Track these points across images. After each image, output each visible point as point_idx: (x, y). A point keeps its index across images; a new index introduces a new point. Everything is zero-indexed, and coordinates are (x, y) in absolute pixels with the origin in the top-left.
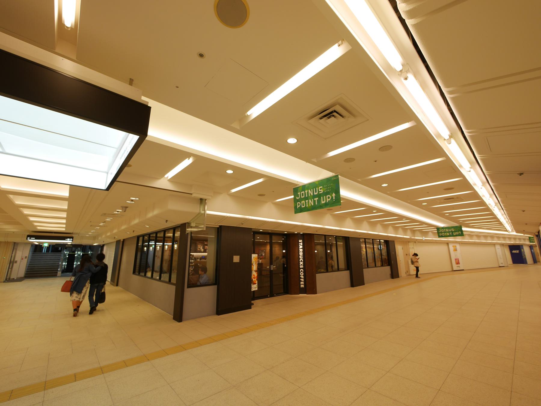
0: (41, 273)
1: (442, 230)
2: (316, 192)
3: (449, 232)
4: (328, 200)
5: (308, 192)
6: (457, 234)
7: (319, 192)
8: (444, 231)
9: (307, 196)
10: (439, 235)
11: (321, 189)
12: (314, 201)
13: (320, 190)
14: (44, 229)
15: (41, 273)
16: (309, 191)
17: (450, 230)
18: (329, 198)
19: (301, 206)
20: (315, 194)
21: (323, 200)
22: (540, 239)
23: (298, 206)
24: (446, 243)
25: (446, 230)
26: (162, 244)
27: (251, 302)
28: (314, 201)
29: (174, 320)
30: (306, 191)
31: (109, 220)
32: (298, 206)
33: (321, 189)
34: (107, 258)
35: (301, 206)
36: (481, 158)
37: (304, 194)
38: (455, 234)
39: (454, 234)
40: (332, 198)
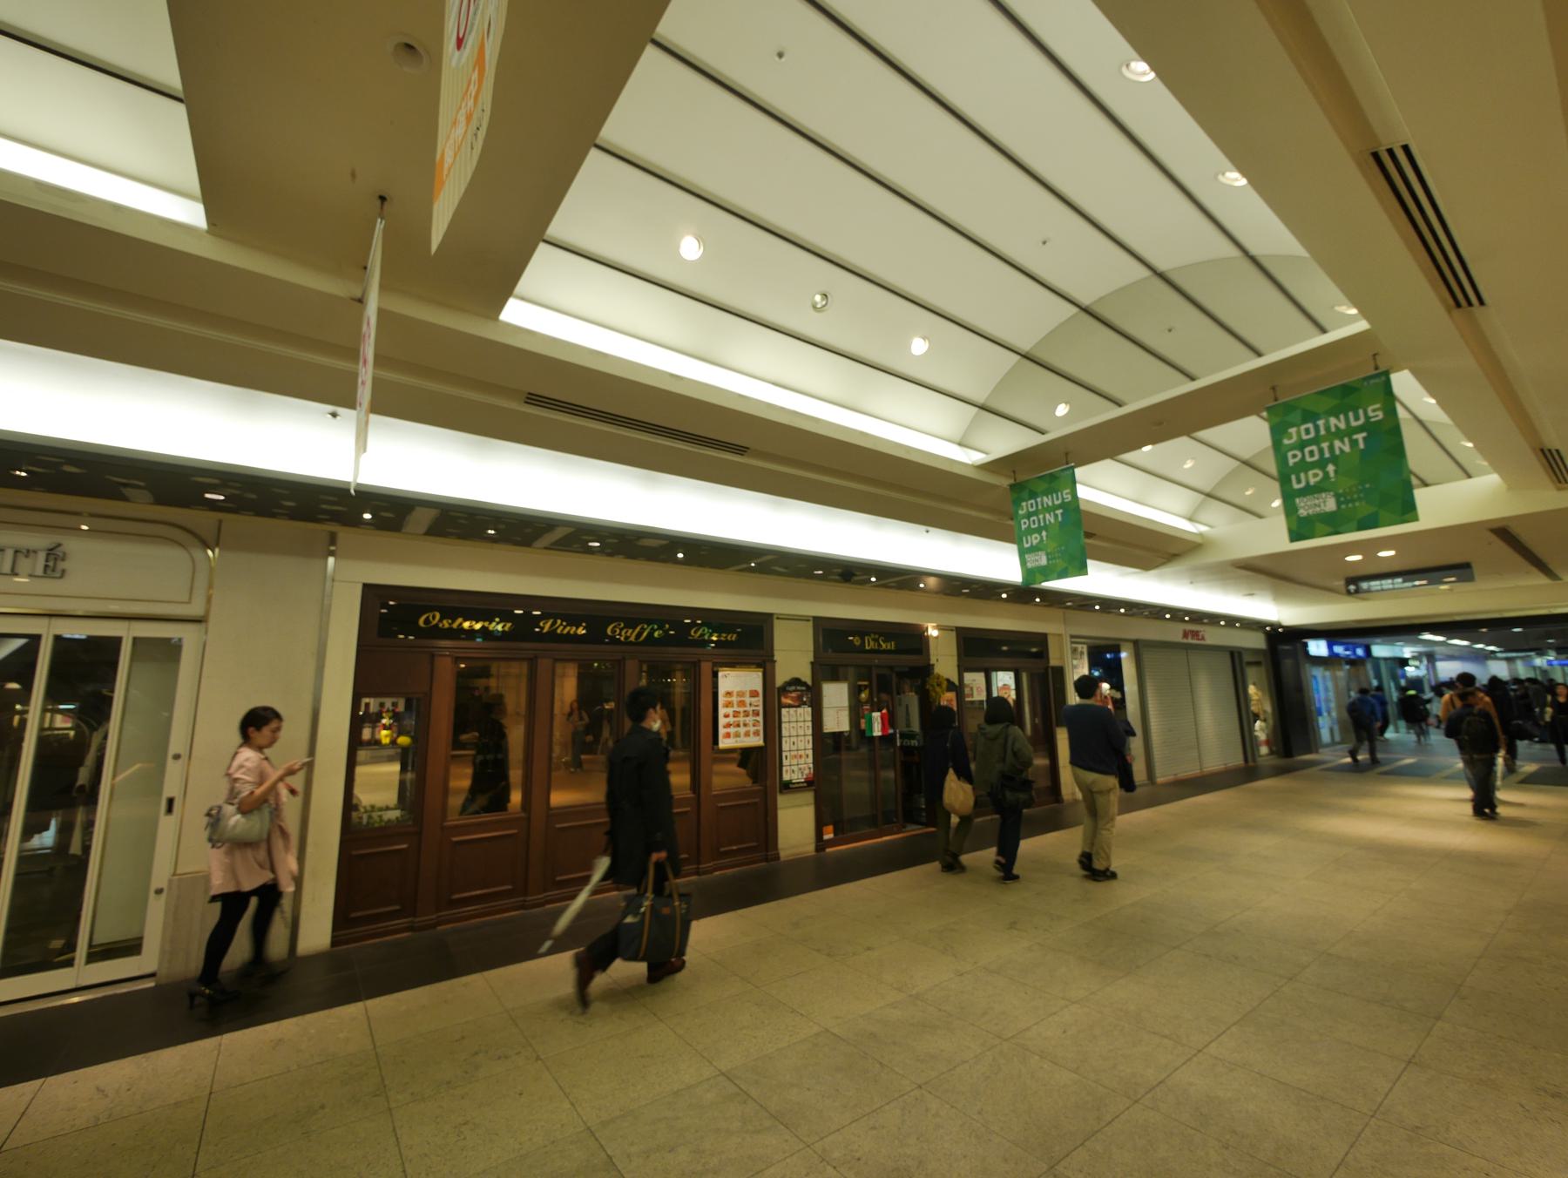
1: (1303, 427)
2: (1058, 499)
3: (1350, 431)
5: (1331, 448)
6: (1312, 481)
7: (1063, 499)
8: (1321, 451)
9: (1042, 524)
10: (1296, 509)
11: (1067, 494)
12: (1056, 516)
13: (1065, 496)
14: (692, 447)
16: (1047, 516)
17: (1357, 419)
18: (1036, 538)
21: (1027, 543)
22: (1565, 466)
24: (382, 208)
25: (1333, 421)
28: (1056, 516)
29: (945, 874)
30: (1041, 516)
31: (62, 707)
33: (1067, 494)
37: (895, 693)
38: (1302, 485)
39: (1296, 486)
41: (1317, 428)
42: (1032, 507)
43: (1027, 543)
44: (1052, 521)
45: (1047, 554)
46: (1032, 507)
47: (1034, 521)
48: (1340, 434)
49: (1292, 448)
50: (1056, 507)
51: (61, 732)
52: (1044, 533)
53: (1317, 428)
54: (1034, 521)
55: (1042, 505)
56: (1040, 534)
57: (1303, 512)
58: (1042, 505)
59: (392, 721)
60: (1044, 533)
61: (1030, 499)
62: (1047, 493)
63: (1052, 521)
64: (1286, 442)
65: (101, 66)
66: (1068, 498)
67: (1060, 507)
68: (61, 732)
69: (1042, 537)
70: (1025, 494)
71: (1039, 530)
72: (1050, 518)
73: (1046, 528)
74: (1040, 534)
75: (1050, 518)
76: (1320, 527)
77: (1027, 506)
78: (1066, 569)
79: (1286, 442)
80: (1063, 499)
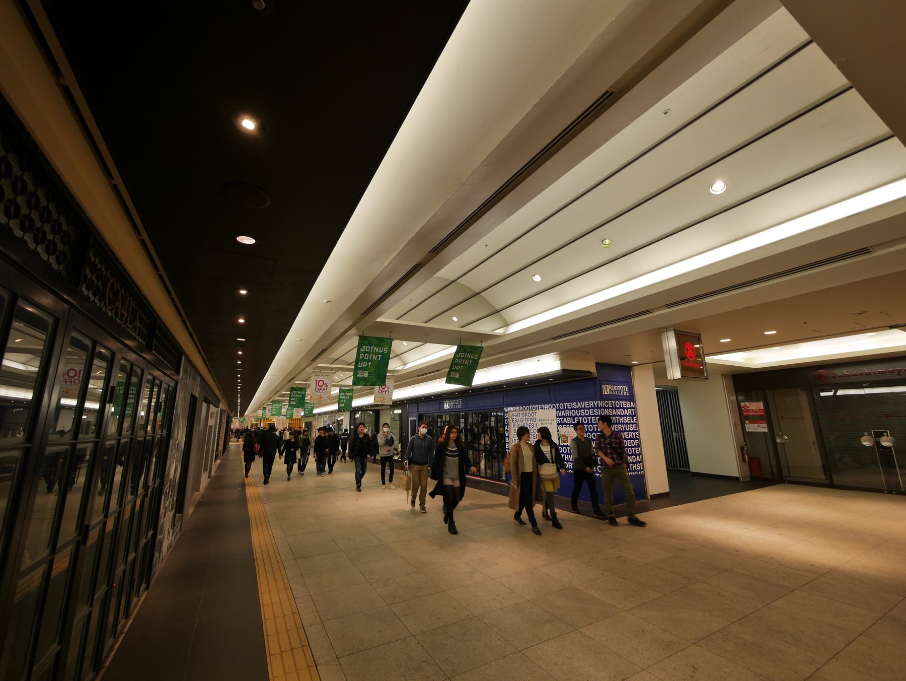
0: (666, 427)
2: (381, 350)
3: (300, 394)
4: (457, 368)
5: (372, 357)
7: (384, 351)
12: (469, 362)
15: (666, 427)
16: (374, 356)
18: (365, 364)
19: (364, 357)
20: (380, 352)
21: (360, 365)
23: (456, 362)
26: (12, 474)
27: (726, 184)
28: (469, 362)
30: (371, 355)
32: (456, 362)
34: (41, 251)
35: (364, 357)
36: (91, 671)
40: (460, 368)
41: (371, 348)
42: (368, 349)
43: (360, 365)
44: (376, 359)
45: (369, 373)
46: (368, 349)
47: (367, 356)
48: (375, 353)
49: (362, 353)
50: (379, 354)
51: (52, 536)
52: (370, 363)
53: (371, 348)
54: (367, 356)
55: (373, 350)
56: (368, 363)
57: (358, 376)
58: (373, 350)
59: (287, 436)
60: (370, 363)
61: (368, 346)
62: (470, 353)
63: (376, 359)
64: (361, 350)
65: (762, 134)
66: (477, 358)
67: (380, 354)
68: (52, 536)
69: (368, 364)
70: (366, 342)
71: (368, 361)
72: (375, 357)
73: (371, 361)
74: (368, 363)
75: (375, 357)
76: (362, 382)
77: (365, 348)
78: (376, 382)
79: (361, 350)
80: (384, 351)
